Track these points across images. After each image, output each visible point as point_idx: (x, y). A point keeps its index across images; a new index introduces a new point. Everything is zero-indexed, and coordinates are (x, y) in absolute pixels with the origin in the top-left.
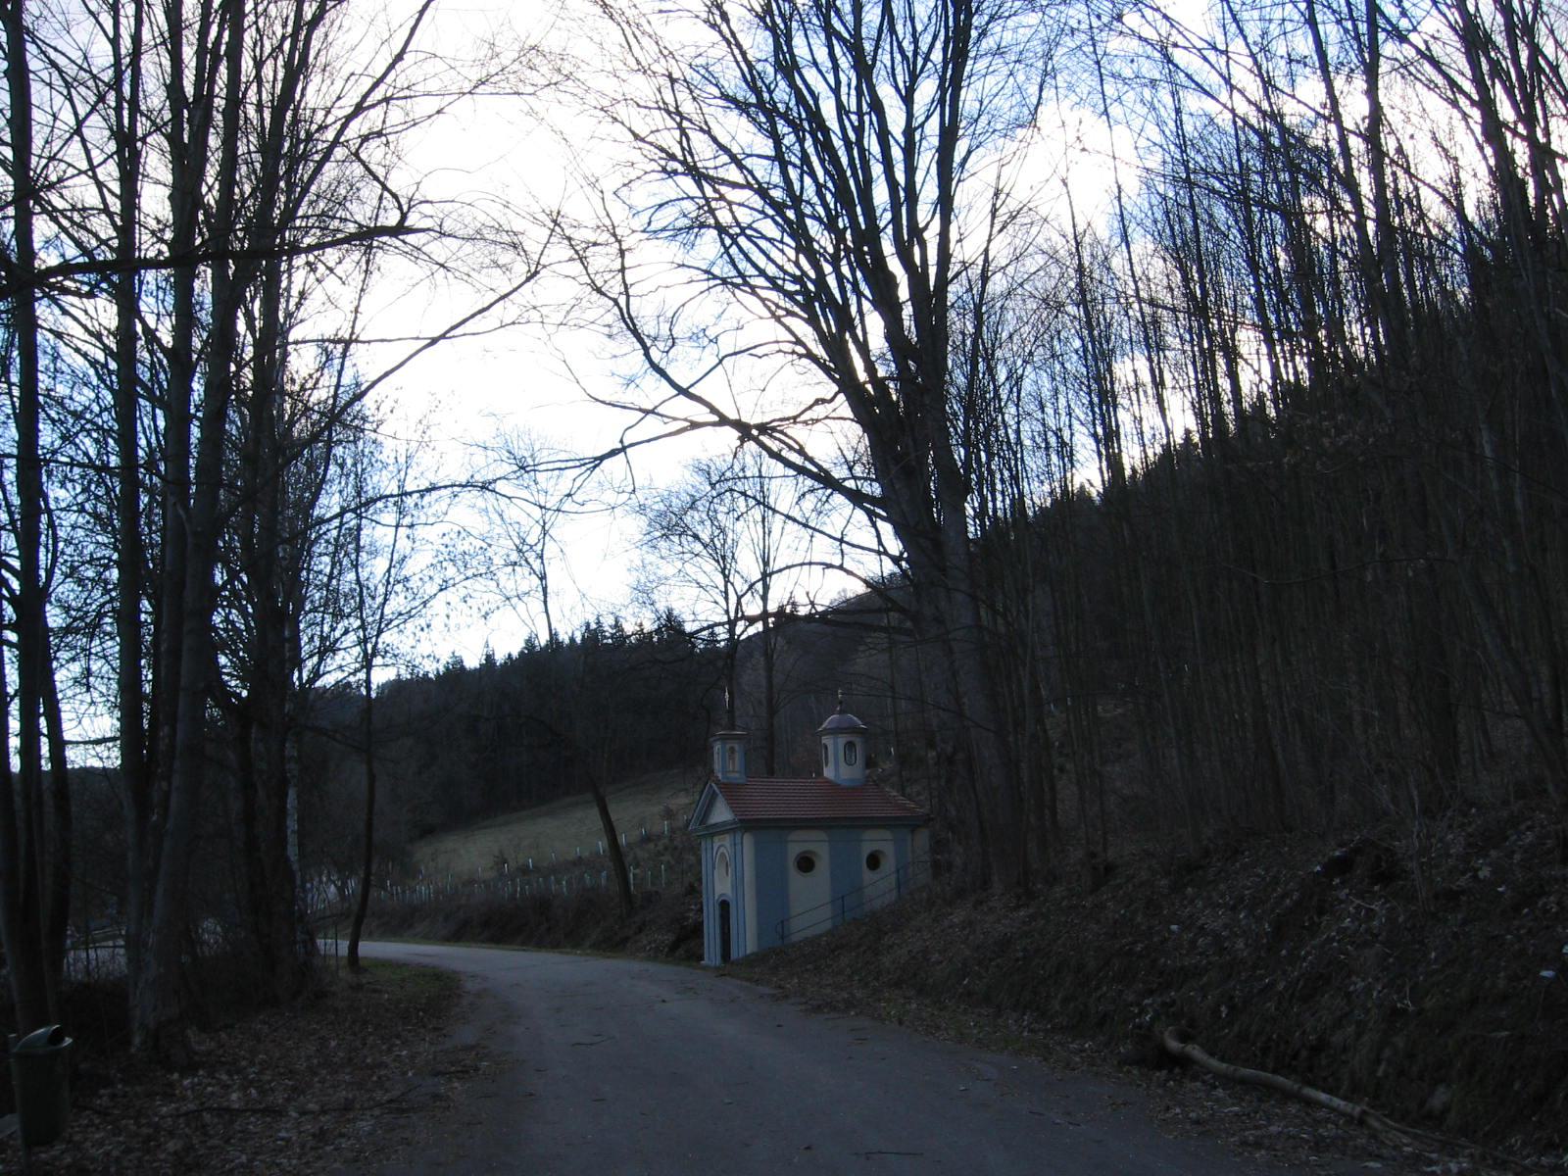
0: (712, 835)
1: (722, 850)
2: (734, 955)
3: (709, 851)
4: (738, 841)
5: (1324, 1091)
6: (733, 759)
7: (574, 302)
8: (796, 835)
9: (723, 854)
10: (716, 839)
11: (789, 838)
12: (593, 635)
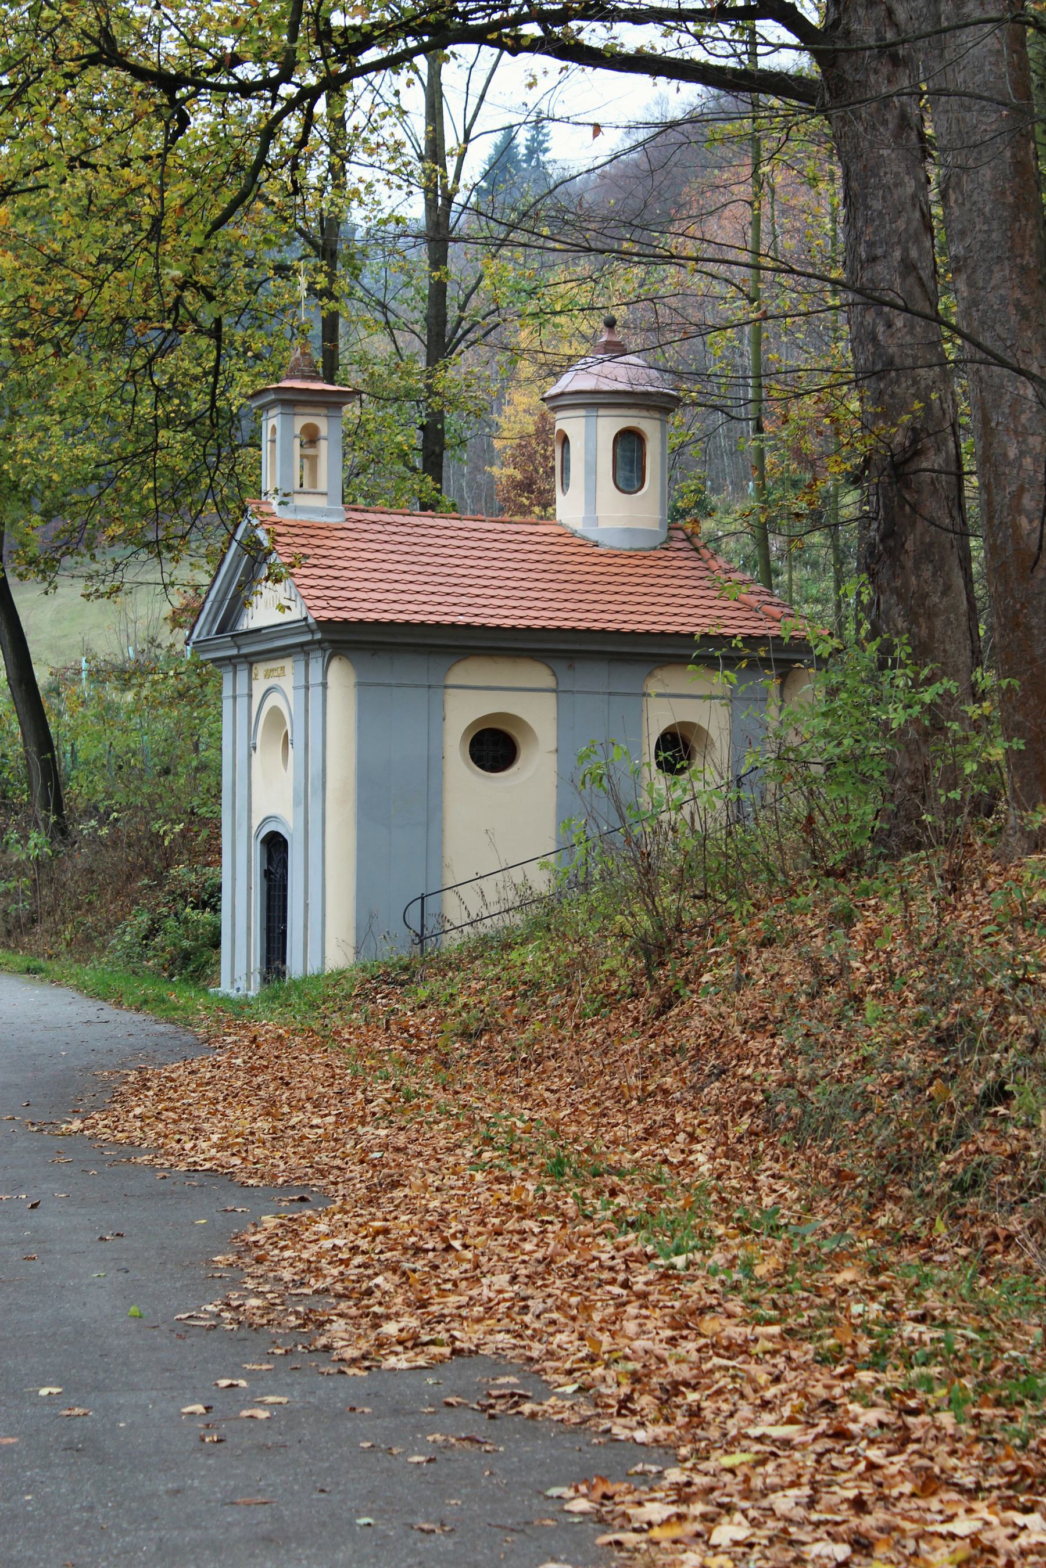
0: (250, 660)
1: (274, 700)
2: (295, 966)
3: (242, 702)
4: (316, 677)
5: (776, 94)
6: (313, 460)
7: (911, 280)
8: (464, 673)
9: (275, 711)
10: (260, 669)
11: (452, 679)
12: (639, 51)
